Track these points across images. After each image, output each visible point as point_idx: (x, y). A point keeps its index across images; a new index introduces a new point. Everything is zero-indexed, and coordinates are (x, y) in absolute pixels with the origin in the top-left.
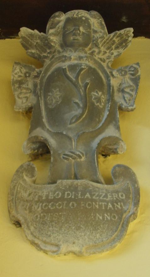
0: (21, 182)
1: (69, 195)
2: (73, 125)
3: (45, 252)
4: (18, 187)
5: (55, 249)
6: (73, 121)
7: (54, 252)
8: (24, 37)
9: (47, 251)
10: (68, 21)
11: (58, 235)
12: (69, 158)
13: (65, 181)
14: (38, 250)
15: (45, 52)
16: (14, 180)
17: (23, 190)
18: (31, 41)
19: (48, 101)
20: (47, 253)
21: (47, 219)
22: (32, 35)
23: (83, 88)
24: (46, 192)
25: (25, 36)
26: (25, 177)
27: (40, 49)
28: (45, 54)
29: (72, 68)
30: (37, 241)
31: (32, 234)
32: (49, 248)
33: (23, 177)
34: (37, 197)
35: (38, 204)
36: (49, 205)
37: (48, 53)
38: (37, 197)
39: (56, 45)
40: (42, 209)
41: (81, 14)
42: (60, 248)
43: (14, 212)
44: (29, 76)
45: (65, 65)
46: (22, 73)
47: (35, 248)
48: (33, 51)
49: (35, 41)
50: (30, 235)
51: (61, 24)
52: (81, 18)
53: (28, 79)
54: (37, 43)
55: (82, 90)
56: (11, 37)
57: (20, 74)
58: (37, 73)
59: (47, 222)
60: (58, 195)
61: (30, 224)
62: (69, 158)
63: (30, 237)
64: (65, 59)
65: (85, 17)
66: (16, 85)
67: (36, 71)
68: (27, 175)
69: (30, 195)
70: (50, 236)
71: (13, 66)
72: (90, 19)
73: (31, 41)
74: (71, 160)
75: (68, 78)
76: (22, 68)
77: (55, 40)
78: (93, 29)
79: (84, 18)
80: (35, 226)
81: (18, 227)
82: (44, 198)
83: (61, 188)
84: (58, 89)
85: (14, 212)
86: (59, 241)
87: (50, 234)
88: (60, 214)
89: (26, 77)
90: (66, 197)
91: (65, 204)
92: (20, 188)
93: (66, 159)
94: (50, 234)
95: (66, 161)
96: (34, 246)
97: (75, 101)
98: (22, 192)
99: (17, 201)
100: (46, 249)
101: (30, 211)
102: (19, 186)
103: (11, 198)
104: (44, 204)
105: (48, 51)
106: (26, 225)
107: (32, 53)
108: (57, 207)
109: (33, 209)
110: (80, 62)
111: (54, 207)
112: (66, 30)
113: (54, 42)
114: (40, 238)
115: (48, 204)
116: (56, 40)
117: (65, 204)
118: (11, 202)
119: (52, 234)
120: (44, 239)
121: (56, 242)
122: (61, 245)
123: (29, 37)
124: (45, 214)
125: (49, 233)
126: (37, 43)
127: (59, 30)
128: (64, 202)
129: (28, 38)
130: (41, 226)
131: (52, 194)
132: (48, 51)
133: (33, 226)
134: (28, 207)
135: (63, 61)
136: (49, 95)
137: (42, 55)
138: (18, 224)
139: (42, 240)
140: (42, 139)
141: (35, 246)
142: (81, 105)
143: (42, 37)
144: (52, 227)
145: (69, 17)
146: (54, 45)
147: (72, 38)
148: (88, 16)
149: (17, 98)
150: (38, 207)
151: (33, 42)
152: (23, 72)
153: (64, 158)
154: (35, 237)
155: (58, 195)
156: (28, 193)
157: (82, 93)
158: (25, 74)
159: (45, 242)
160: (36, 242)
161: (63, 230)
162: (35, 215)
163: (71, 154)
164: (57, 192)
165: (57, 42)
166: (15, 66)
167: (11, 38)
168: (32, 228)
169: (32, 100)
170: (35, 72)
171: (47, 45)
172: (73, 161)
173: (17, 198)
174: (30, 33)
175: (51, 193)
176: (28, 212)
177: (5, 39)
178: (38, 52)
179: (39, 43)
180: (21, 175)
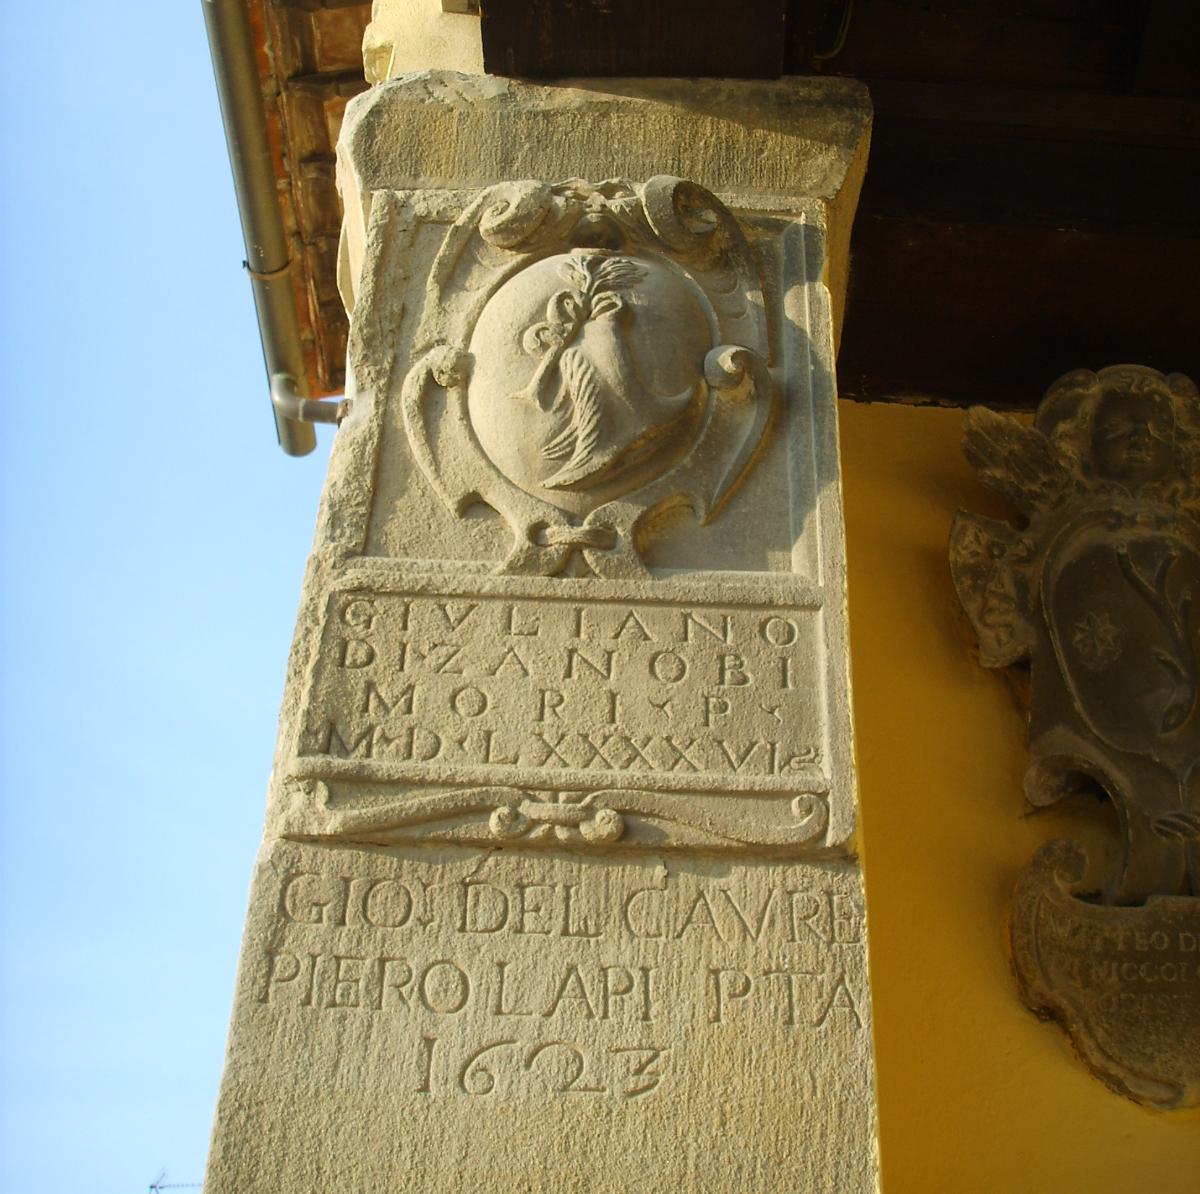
0: (1047, 895)
1: (1191, 945)
2: (1173, 734)
3: (1136, 1100)
4: (1038, 909)
5: (1165, 1094)
6: (1173, 721)
7: (1161, 1102)
8: (977, 432)
9: (1141, 1098)
10: (1112, 402)
11: (1173, 1056)
12: (1174, 832)
13: (1173, 898)
14: (1114, 1091)
15: (1034, 479)
16: (1029, 888)
17: (1053, 916)
18: (992, 443)
19: (1080, 646)
20: (1141, 1102)
21: (1140, 1011)
22: (998, 430)
23: (1179, 619)
24: (1125, 931)
25: (980, 430)
26: (1058, 882)
27: (1017, 470)
28: (1035, 488)
29: (1145, 550)
30: (1113, 1070)
31: (1100, 1048)
32: (1149, 1091)
33: (1051, 880)
34: (1098, 941)
35: (1106, 962)
36: (1139, 968)
37: (1044, 484)
38: (1098, 941)
39: (1072, 467)
40: (1121, 979)
41: (1148, 386)
42: (1180, 1093)
43: (1038, 983)
44: (1000, 556)
45: (1121, 540)
46: (980, 544)
47: (1103, 1085)
48: (999, 474)
49: (1004, 445)
50: (1095, 1053)
51: (1088, 408)
52: (1150, 395)
53: (997, 563)
54: (1011, 452)
55: (1179, 624)
56: (887, 397)
57: (973, 547)
58: (1029, 550)
59: (1140, 1017)
60: (1160, 939)
61: (1093, 1020)
62: (1174, 832)
63: (1097, 1059)
64: (1118, 521)
65: (1160, 395)
66: (964, 579)
67: (1025, 544)
68: (1061, 877)
69: (1074, 932)
70: (1152, 1058)
71: (954, 522)
72: (1170, 399)
73: (992, 443)
74: (1179, 837)
75: (1136, 584)
76: (980, 531)
77: (1070, 453)
78: (1178, 428)
79: (1157, 398)
80: (1106, 1026)
81: (1045, 1020)
82: (1120, 947)
83: (1164, 919)
84: (1107, 615)
85: (1038, 983)
86: (1179, 1075)
87: (1152, 1054)
88: (1175, 997)
89: (992, 556)
90: (1182, 949)
91: (1183, 970)
92: (1045, 910)
93: (1167, 834)
94: (1152, 1054)
95: (1164, 839)
96: (1102, 1080)
97: (1163, 658)
98: (1052, 923)
99: (1042, 951)
100: (1141, 1093)
101: (1087, 984)
102: (1042, 906)
103: (1026, 941)
104: (1125, 965)
105: (1044, 478)
106: (1081, 1025)
107: (995, 478)
108: (1165, 977)
109: (1093, 977)
110: (1158, 533)
111: (1156, 977)
112: (1106, 426)
113: (1070, 458)
114: (1126, 1062)
115: (1136, 967)
116: (1073, 452)
117: (1183, 970)
118: (1026, 952)
119: (1156, 1054)
120: (1138, 1066)
121: (1172, 1077)
122: (1184, 1086)
123: (989, 434)
124: (1133, 996)
125: (1149, 1051)
126: (1011, 452)
127: (1085, 426)
128: (1181, 964)
129: (987, 437)
130: (1123, 1028)
131: (1142, 937)
132: (1044, 478)
133: (1103, 1028)
134: (1076, 969)
135: (1112, 528)
136: (1082, 630)
137: (1025, 488)
138: (1049, 1013)
139: (1131, 1070)
140: (1086, 766)
141: (1105, 1080)
142: (1184, 673)
143: (1029, 438)
144: (1157, 1035)
145: (1114, 390)
146: (1068, 467)
147: (1125, 456)
148: (1164, 388)
149: (979, 627)
150: (1109, 974)
151: (998, 448)
152: (983, 542)
153: (1160, 831)
154: (1109, 1058)
155: (1160, 939)
156: (1068, 928)
157: (1180, 635)
158: (989, 548)
159: (1138, 1075)
160: (1112, 1072)
161: (1187, 1045)
162: (1104, 996)
163: (1181, 822)
164: (1157, 933)
165: (1076, 458)
166: (959, 523)
167: (888, 401)
168: (1100, 1033)
169: (1027, 640)
170: (1021, 547)
171: (1039, 457)
172: (1184, 839)
173: (1040, 942)
174: (995, 424)
175: (1137, 934)
176: (1078, 984)
177: (869, 402)
178: (1012, 480)
179: (1017, 453)
180: (1046, 875)
